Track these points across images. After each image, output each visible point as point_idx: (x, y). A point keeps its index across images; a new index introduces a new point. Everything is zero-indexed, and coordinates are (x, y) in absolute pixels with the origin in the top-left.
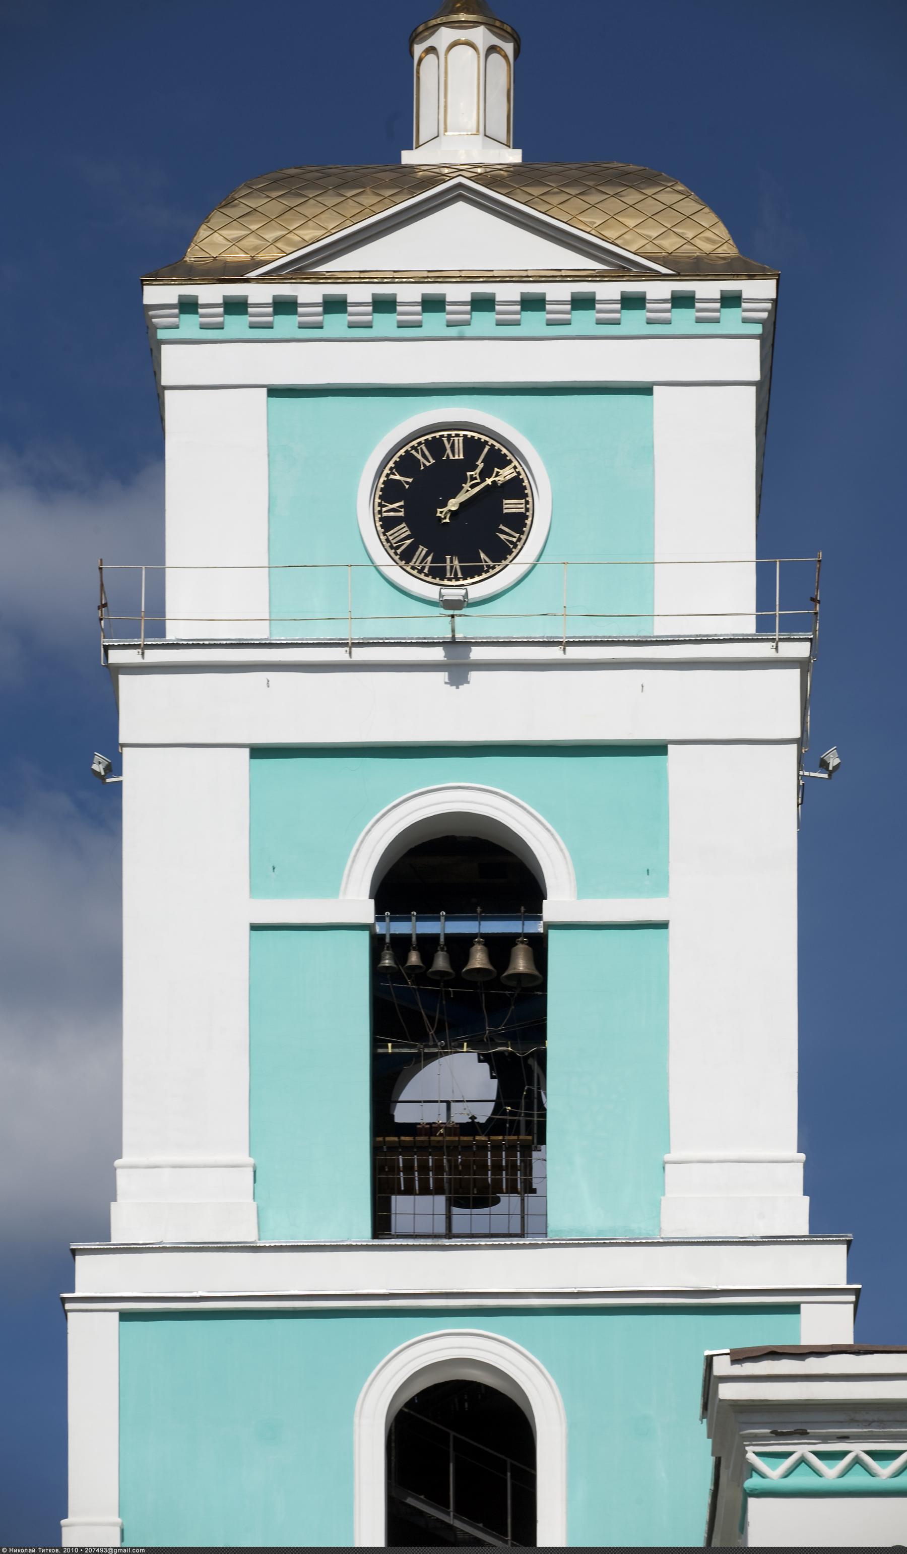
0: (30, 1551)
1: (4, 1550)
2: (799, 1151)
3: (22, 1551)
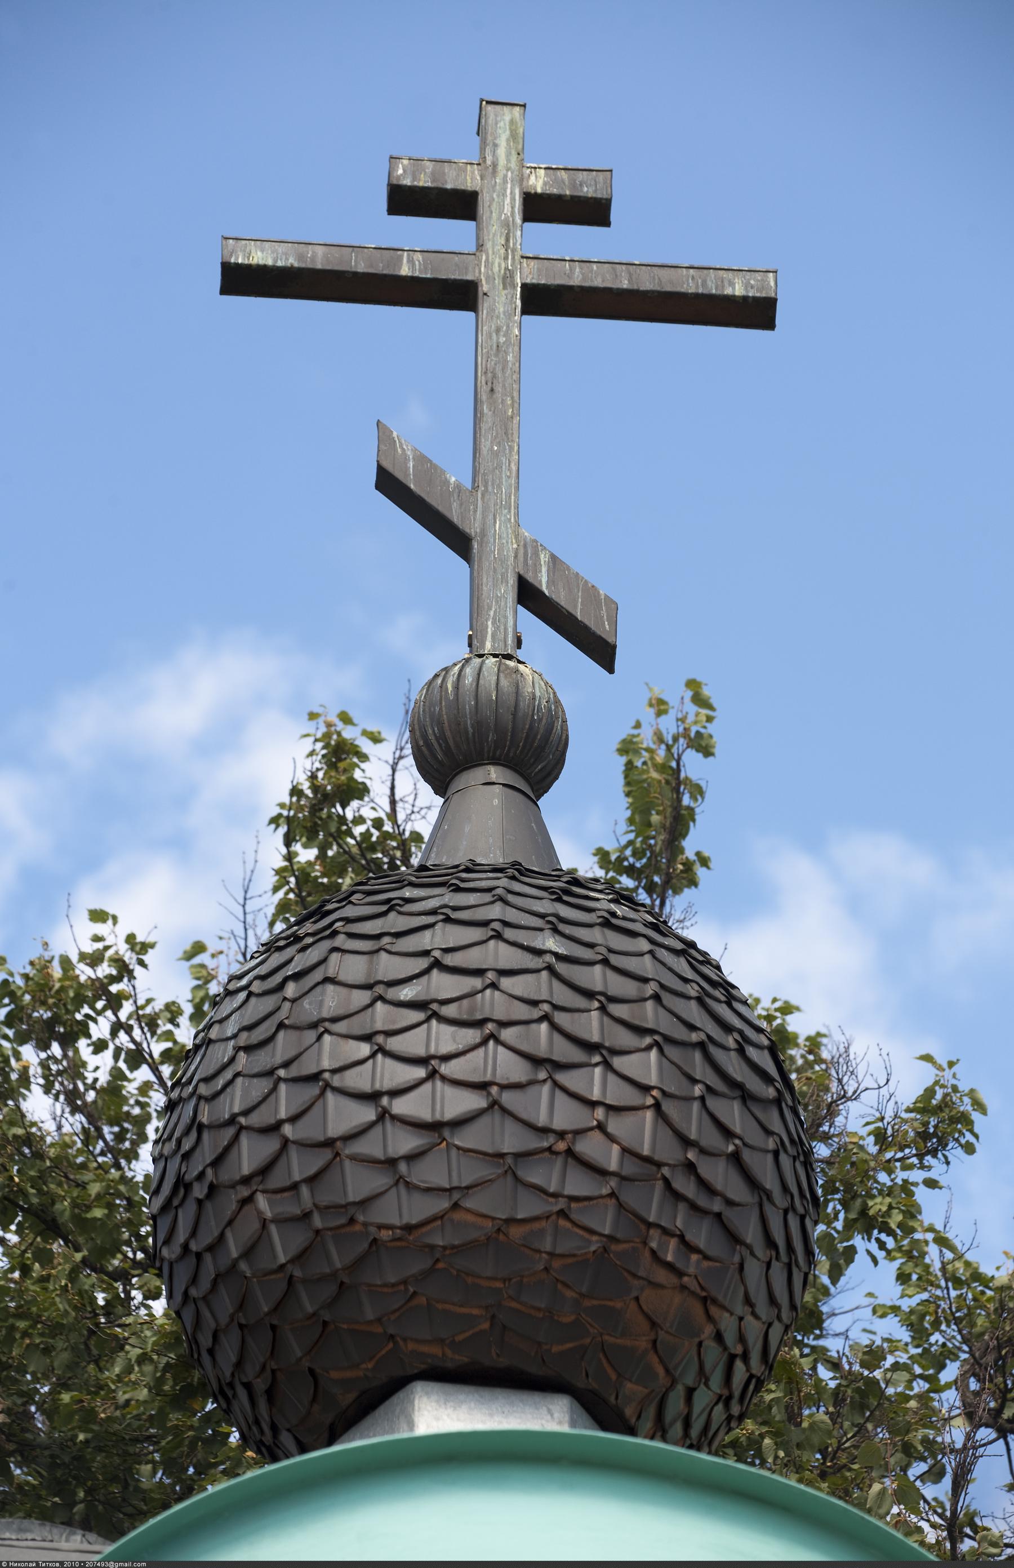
0: (31, 1565)
1: (4, 1565)
2: (412, 833)
3: (23, 1565)
